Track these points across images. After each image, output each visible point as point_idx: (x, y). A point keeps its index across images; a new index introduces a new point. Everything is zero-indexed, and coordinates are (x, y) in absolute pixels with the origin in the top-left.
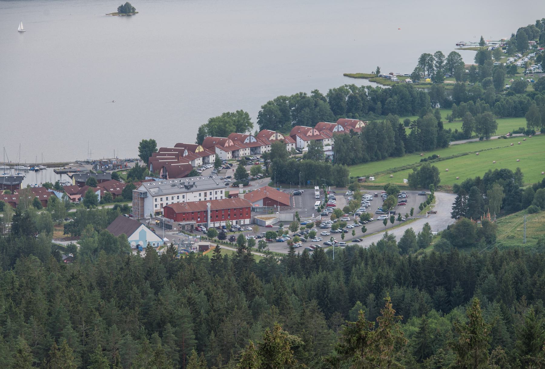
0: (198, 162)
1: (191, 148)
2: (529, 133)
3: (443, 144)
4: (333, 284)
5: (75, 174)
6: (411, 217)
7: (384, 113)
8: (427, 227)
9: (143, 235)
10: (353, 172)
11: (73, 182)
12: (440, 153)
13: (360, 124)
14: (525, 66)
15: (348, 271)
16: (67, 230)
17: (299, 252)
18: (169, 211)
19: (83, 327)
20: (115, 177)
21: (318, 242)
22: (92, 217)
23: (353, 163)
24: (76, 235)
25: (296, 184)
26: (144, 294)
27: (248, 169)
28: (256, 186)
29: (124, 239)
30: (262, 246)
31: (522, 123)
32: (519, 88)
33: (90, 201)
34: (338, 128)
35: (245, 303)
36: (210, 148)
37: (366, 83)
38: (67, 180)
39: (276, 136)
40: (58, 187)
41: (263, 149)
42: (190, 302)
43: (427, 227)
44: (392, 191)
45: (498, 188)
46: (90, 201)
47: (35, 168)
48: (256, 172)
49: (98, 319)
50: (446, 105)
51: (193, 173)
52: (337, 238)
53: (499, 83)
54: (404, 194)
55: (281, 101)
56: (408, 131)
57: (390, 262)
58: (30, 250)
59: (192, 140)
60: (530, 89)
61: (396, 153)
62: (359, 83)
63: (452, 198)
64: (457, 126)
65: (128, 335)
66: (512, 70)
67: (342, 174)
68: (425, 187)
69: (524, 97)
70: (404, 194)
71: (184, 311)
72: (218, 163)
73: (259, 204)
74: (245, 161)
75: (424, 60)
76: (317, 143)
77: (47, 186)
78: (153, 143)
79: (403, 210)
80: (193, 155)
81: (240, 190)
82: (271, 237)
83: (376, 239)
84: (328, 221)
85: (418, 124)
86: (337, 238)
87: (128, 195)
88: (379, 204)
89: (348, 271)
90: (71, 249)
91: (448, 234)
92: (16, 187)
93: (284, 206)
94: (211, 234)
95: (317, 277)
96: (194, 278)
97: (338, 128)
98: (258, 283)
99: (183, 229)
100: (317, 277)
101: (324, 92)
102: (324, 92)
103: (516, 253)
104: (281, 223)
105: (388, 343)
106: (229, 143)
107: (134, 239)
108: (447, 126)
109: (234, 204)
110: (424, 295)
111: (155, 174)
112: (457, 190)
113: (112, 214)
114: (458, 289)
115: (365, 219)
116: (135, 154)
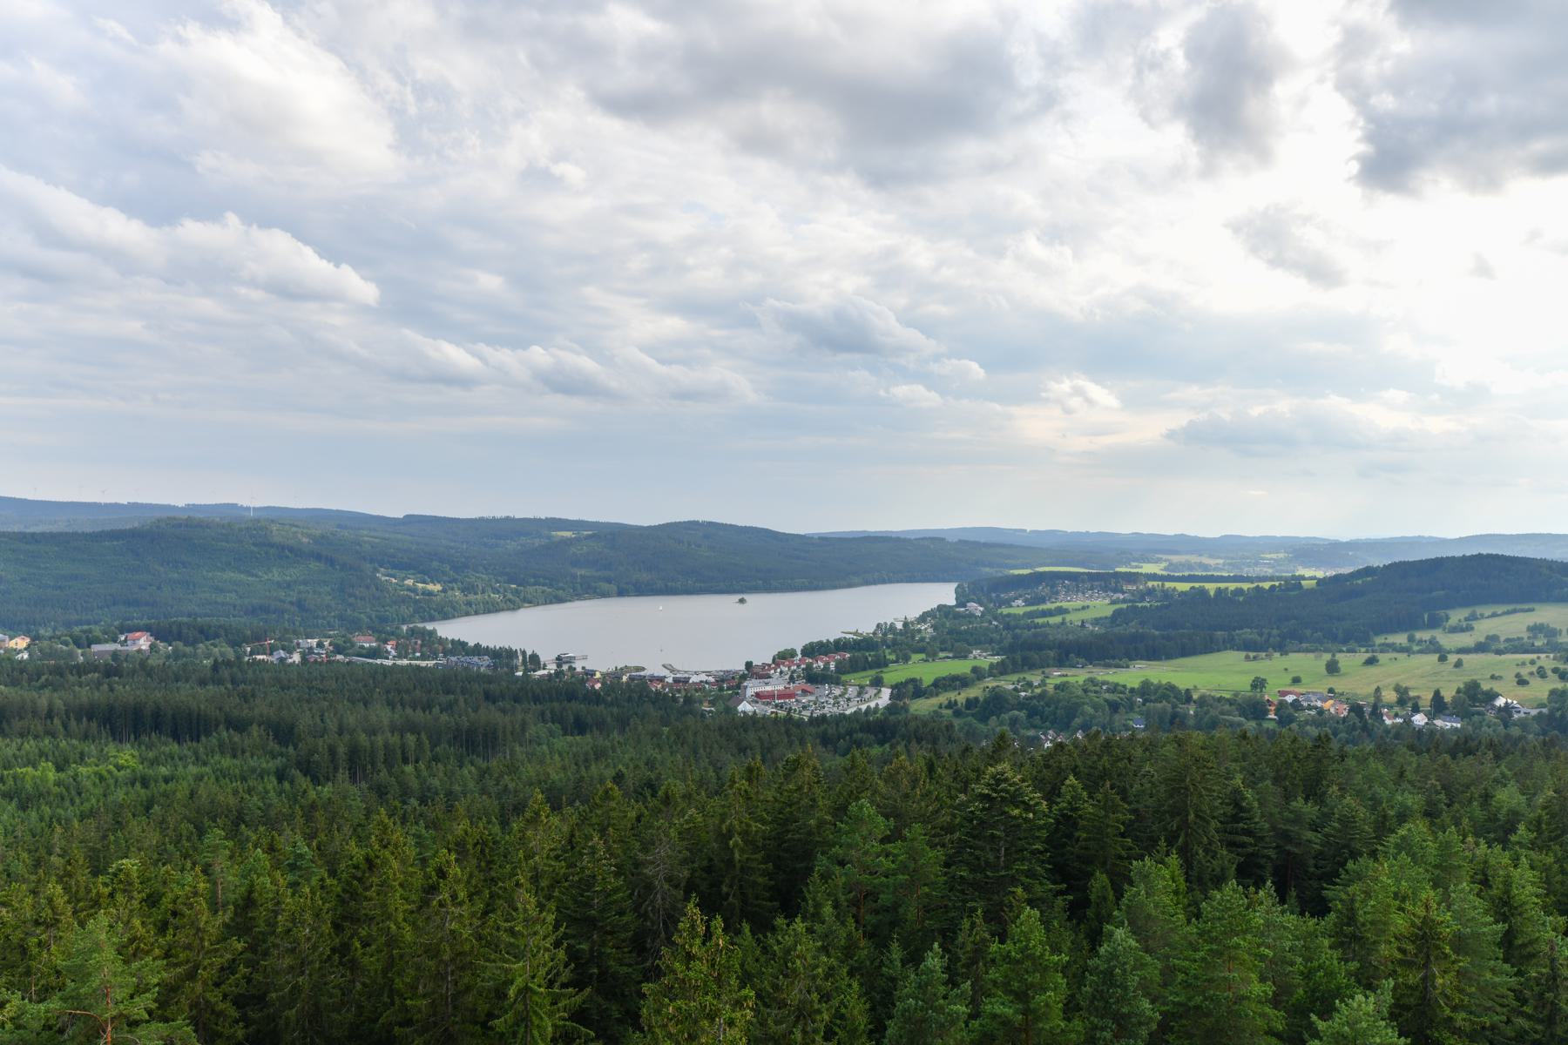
0: (772, 671)
1: (769, 665)
2: (926, 661)
4: (830, 731)
5: (715, 677)
6: (870, 699)
7: (859, 650)
8: (877, 705)
9: (744, 706)
10: (844, 678)
12: (885, 670)
13: (847, 655)
14: (926, 629)
15: (837, 725)
17: (815, 715)
18: (757, 695)
19: (708, 750)
20: (733, 678)
21: (826, 711)
23: (844, 673)
24: (714, 705)
26: (739, 734)
27: (795, 675)
29: (736, 707)
30: (800, 712)
31: (923, 656)
32: (923, 639)
33: (721, 689)
34: (838, 657)
35: (786, 740)
36: (778, 665)
37: (851, 636)
38: (711, 679)
40: (706, 682)
41: (803, 666)
42: (760, 739)
43: (877, 705)
44: (862, 687)
45: (910, 687)
46: (721, 689)
47: (696, 673)
49: (716, 746)
50: (888, 647)
51: (770, 677)
52: (835, 709)
54: (867, 688)
55: (812, 644)
56: (870, 659)
57: (857, 721)
58: (691, 712)
59: (770, 661)
60: (928, 640)
61: (864, 669)
62: (848, 636)
63: (890, 691)
64: (893, 657)
65: (496, 829)
66: (919, 631)
67: (838, 678)
68: (877, 686)
69: (924, 644)
70: (867, 688)
71: (757, 744)
72: (781, 672)
73: (800, 692)
74: (794, 671)
75: (879, 626)
76: (827, 664)
77: (701, 682)
78: (751, 663)
79: (867, 696)
82: (804, 708)
83: (853, 710)
84: (832, 701)
85: (875, 656)
86: (835, 709)
87: (738, 687)
88: (856, 693)
89: (837, 725)
90: (710, 712)
91: (887, 708)
93: (811, 693)
94: (776, 706)
95: (822, 728)
96: (764, 728)
97: (838, 657)
98: (794, 730)
99: (763, 704)
100: (822, 728)
101: (832, 640)
102: (832, 640)
103: (916, 718)
104: (809, 701)
105: (808, 766)
106: (787, 663)
107: (740, 708)
108: (888, 657)
110: (873, 737)
111: (752, 677)
112: (893, 687)
113: (731, 696)
115: (849, 700)
116: (743, 668)
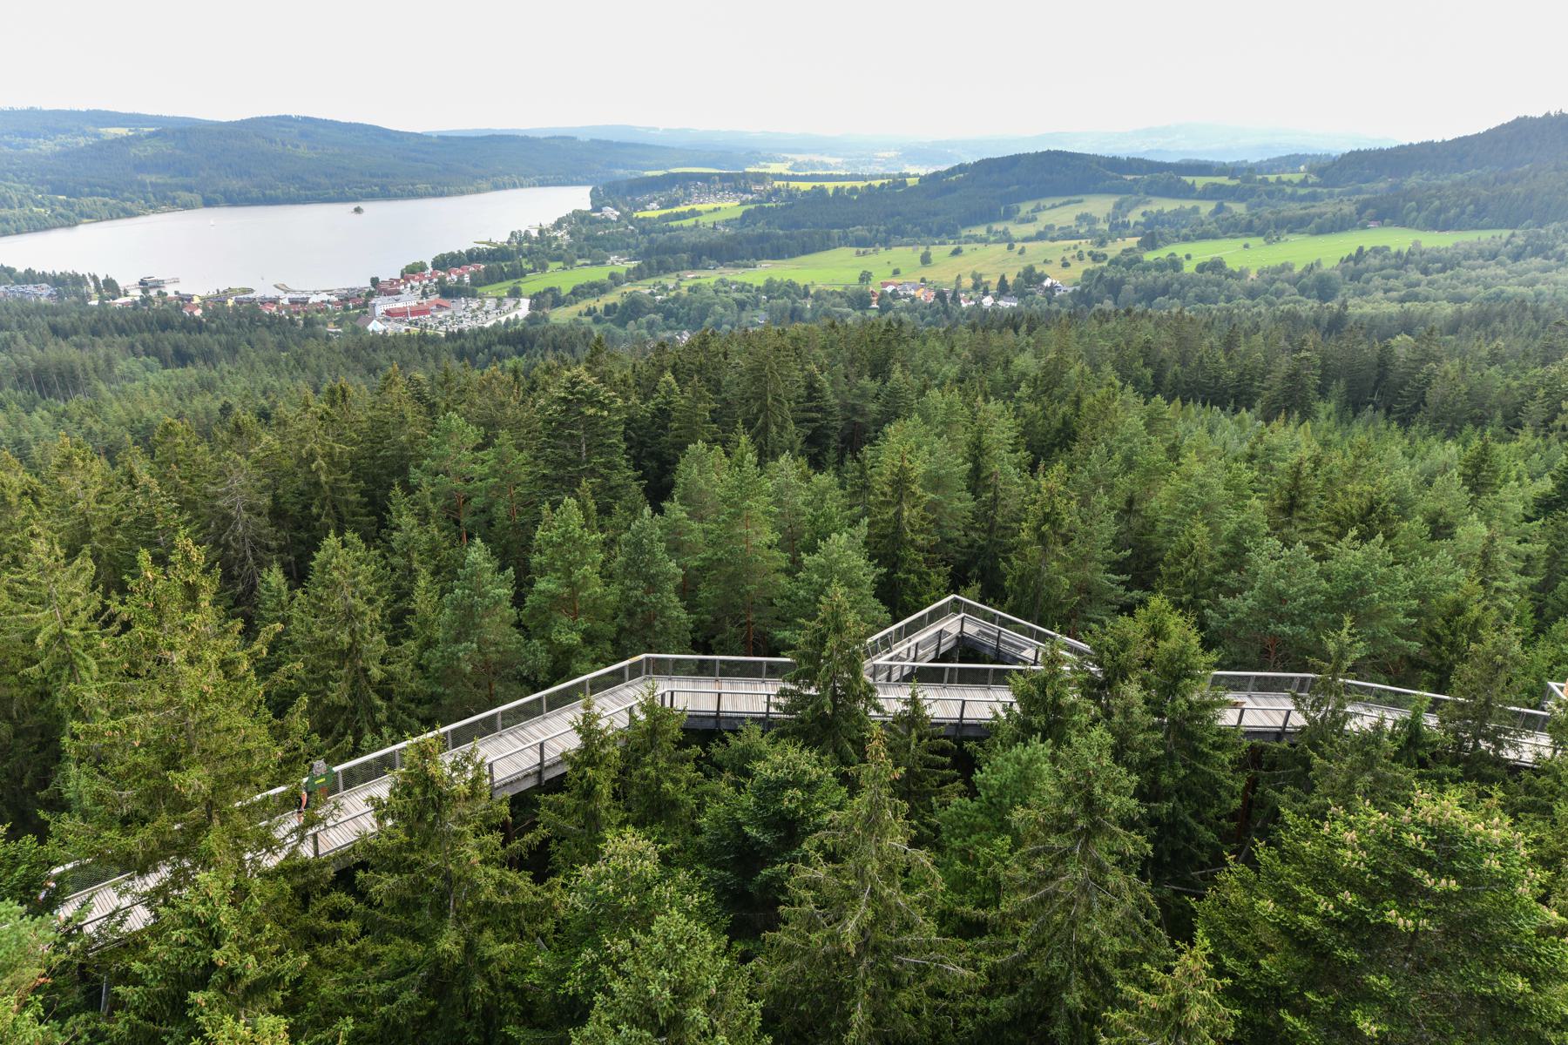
0: (402, 287)
1: (398, 281)
3: (523, 275)
6: (509, 311)
10: (480, 290)
11: (336, 299)
13: (483, 267)
16: (335, 323)
18: (388, 312)
22: (348, 317)
23: (480, 286)
24: (340, 326)
25: (452, 297)
27: (428, 290)
28: (432, 298)
31: (561, 264)
33: (346, 309)
34: (472, 269)
36: (408, 280)
38: (334, 298)
39: (441, 273)
40: (328, 302)
44: (500, 299)
45: (549, 296)
46: (346, 309)
48: (431, 291)
50: (525, 256)
51: (400, 293)
53: (549, 245)
55: (442, 256)
61: (501, 280)
62: (481, 246)
64: (530, 266)
66: (556, 238)
72: (412, 288)
74: (426, 286)
75: (513, 234)
79: (506, 308)
80: (399, 285)
81: (425, 300)
82: (441, 323)
83: (492, 323)
87: (366, 305)
88: (494, 305)
92: (306, 303)
94: (410, 323)
97: (472, 269)
107: (370, 327)
109: (421, 307)
111: (379, 294)
112: (532, 298)
114: (528, 345)
115: (487, 312)
116: (369, 284)
